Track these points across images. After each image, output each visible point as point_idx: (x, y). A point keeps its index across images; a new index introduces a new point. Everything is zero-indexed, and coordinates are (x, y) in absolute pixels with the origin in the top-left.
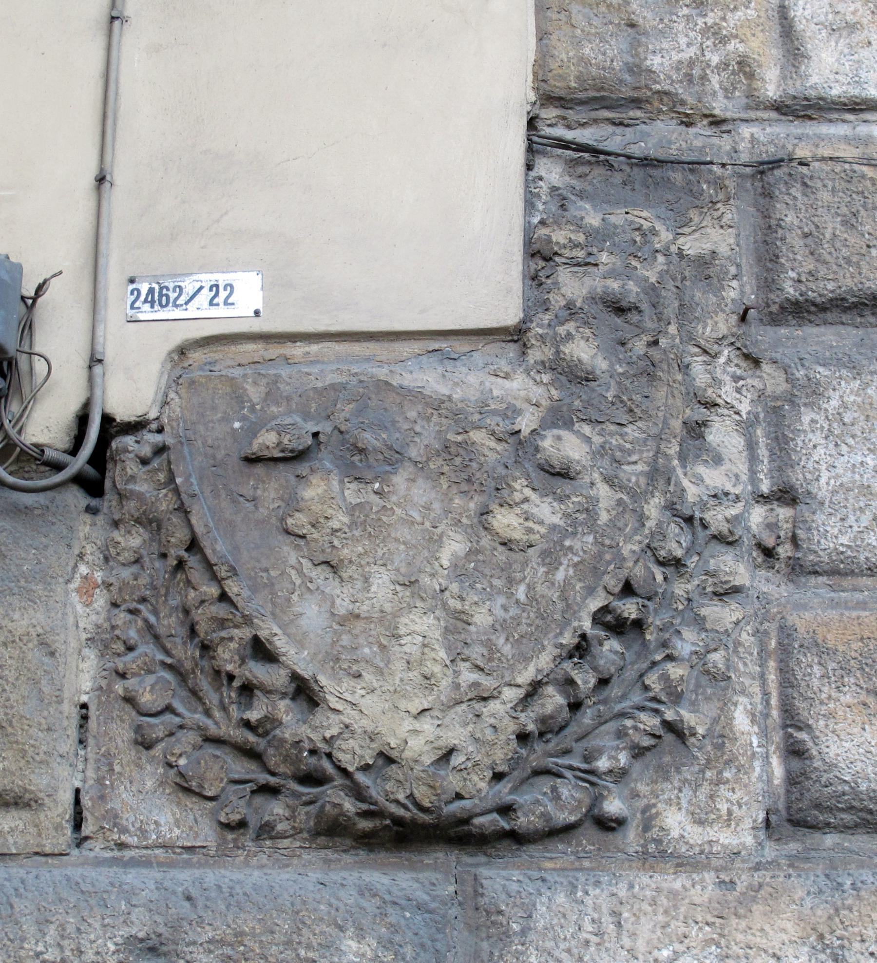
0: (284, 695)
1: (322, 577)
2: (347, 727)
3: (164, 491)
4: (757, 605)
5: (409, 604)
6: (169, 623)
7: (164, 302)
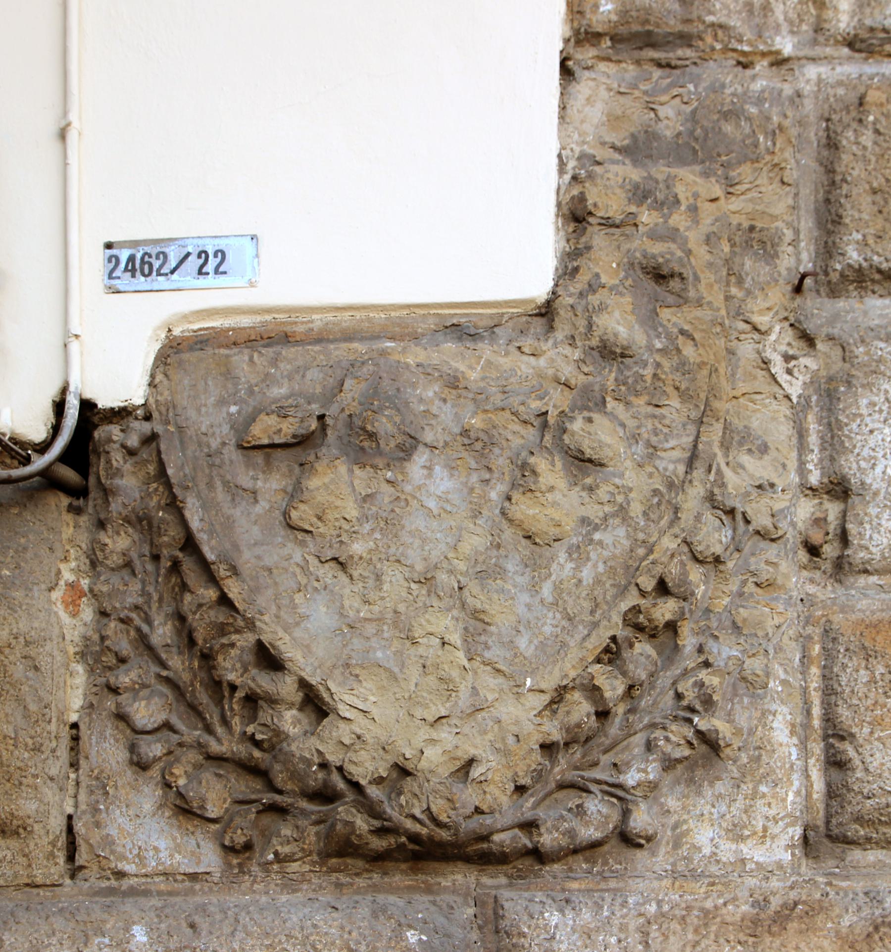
0: (291, 705)
1: (330, 576)
2: (359, 737)
3: (155, 485)
4: (800, 607)
5: (425, 604)
6: (162, 632)
7: (146, 271)
